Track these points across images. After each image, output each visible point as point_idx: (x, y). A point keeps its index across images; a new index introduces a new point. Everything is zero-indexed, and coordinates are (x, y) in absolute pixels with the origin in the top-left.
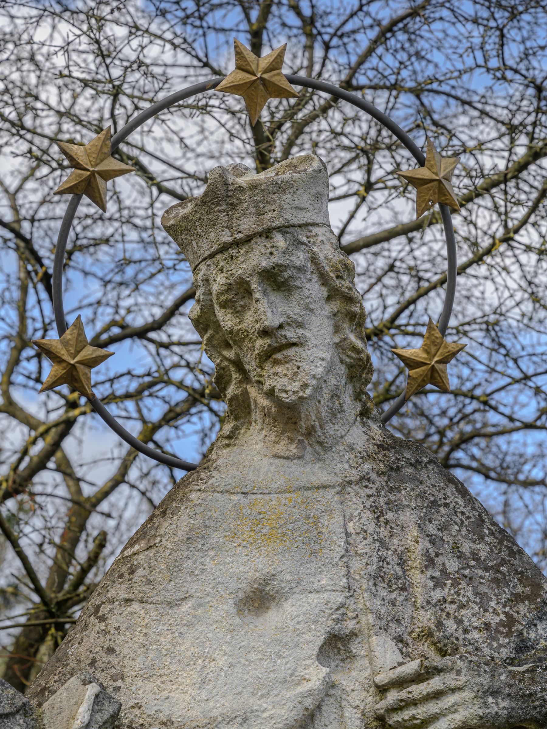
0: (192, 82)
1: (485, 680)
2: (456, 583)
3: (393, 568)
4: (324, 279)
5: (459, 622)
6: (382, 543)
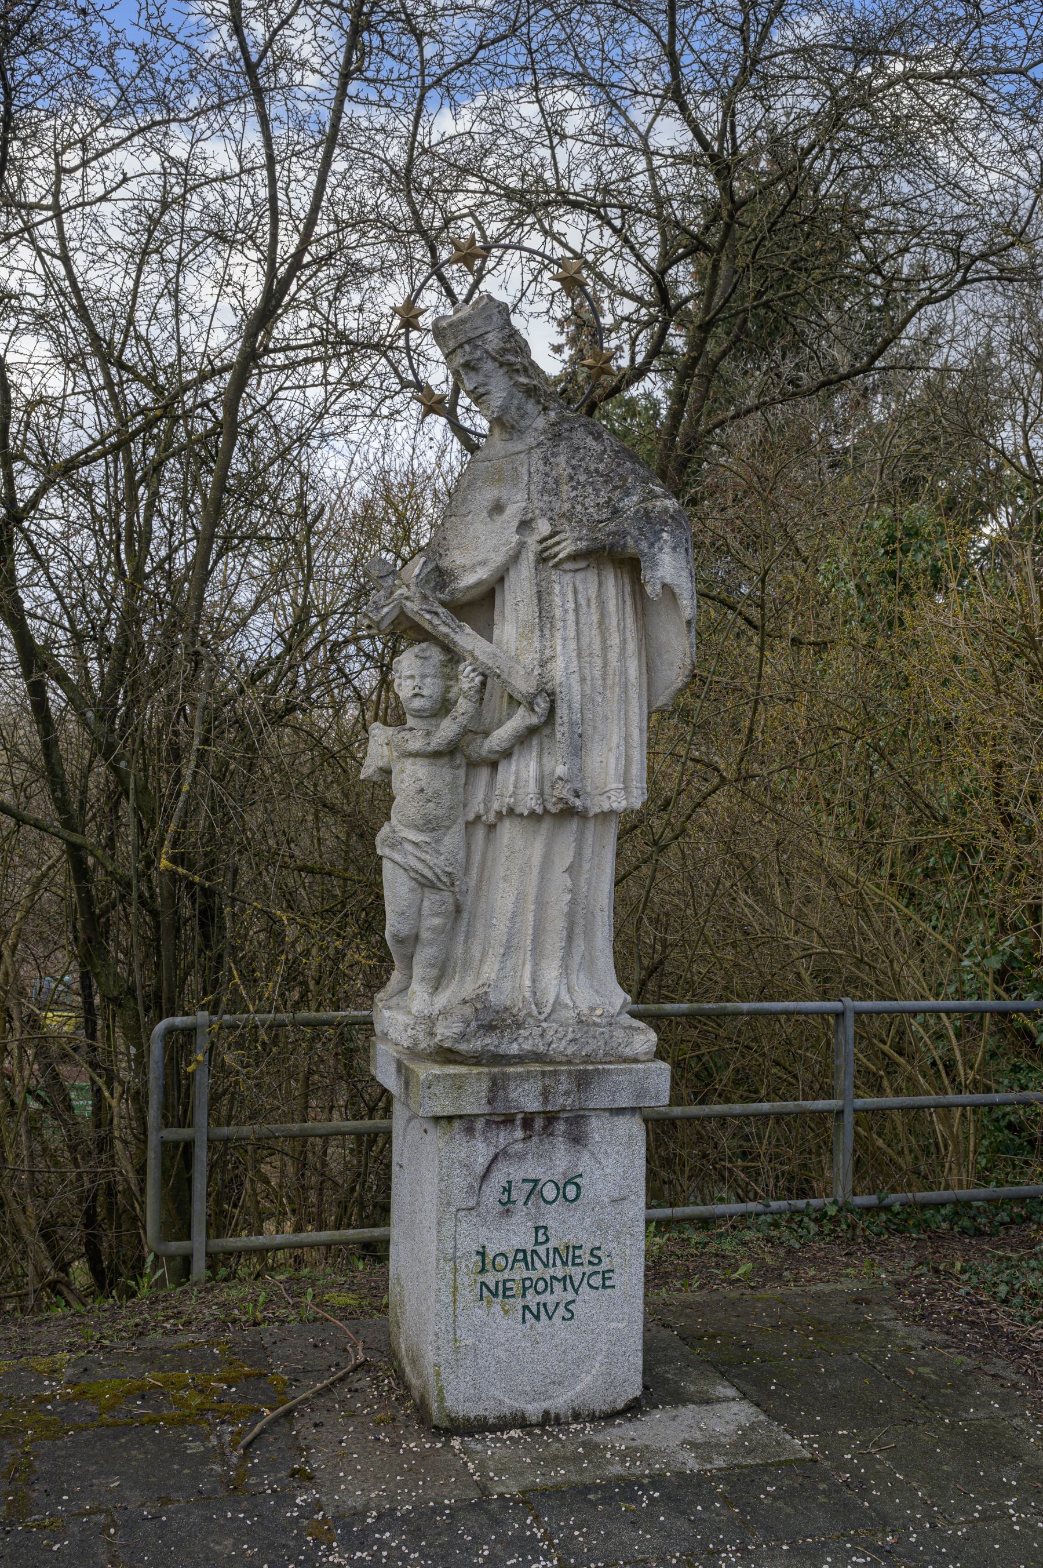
0: (62, 719)
1: (576, 534)
2: (584, 486)
3: (551, 485)
4: (494, 359)
5: (583, 505)
6: (547, 475)
